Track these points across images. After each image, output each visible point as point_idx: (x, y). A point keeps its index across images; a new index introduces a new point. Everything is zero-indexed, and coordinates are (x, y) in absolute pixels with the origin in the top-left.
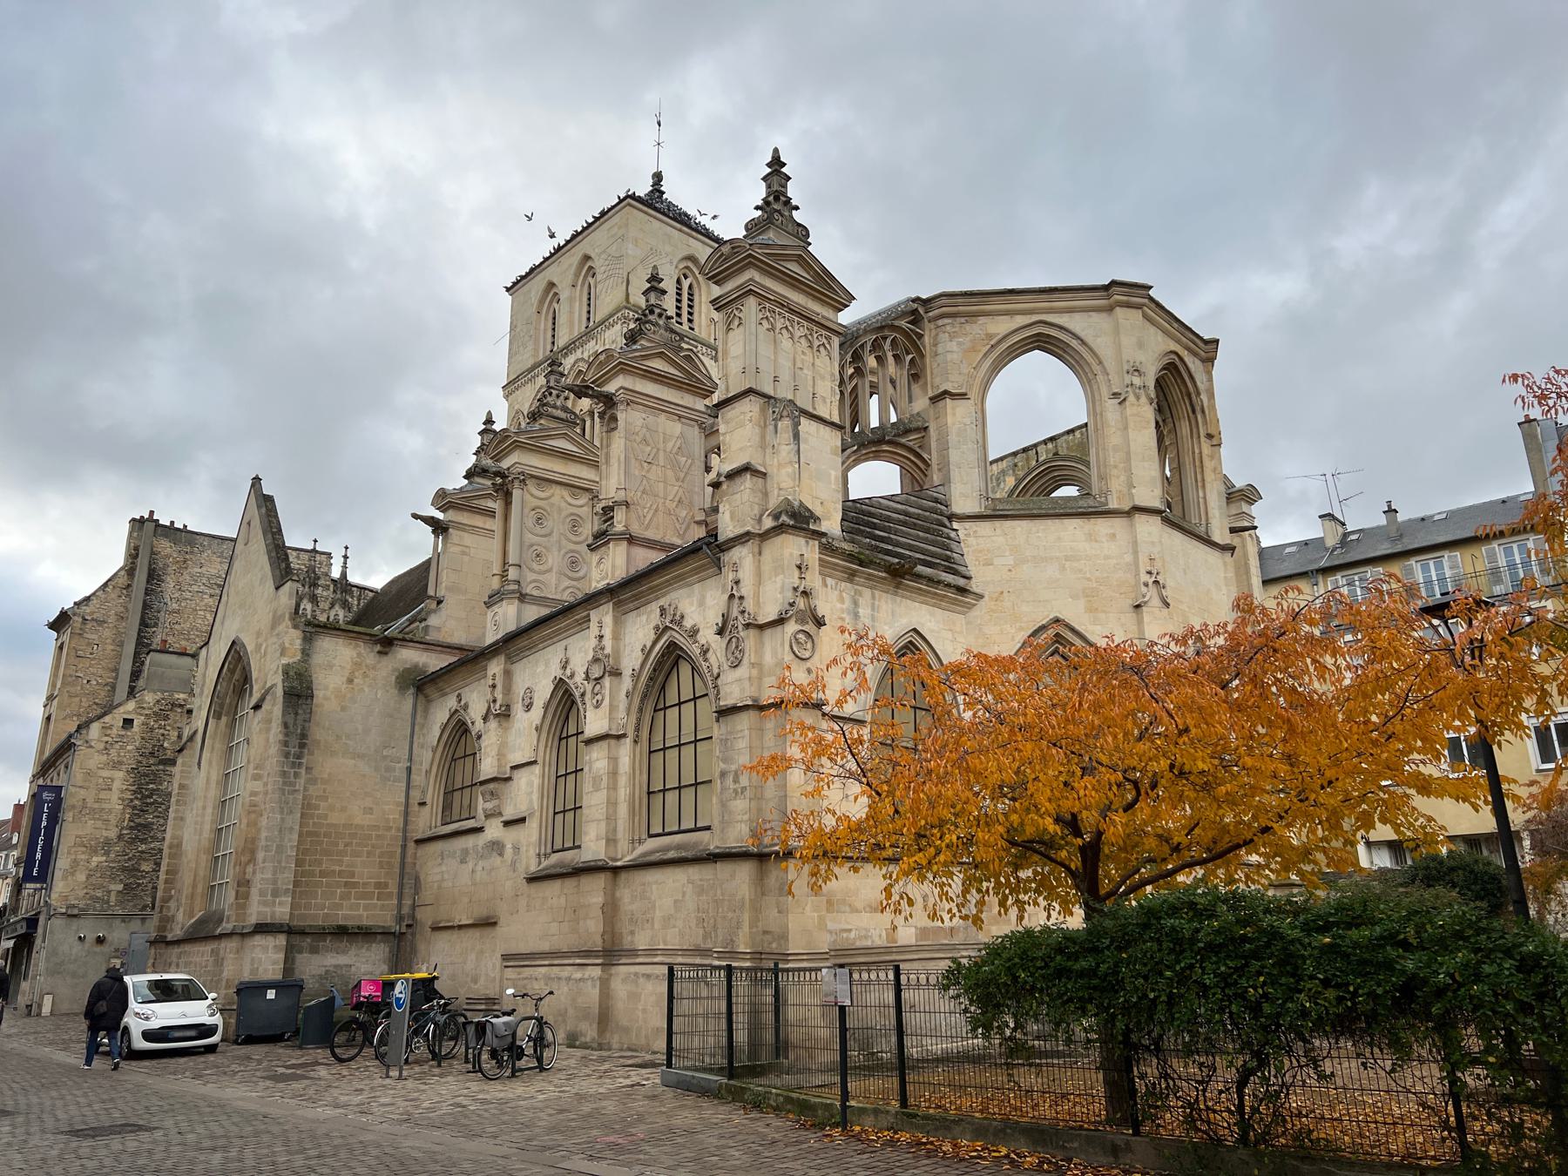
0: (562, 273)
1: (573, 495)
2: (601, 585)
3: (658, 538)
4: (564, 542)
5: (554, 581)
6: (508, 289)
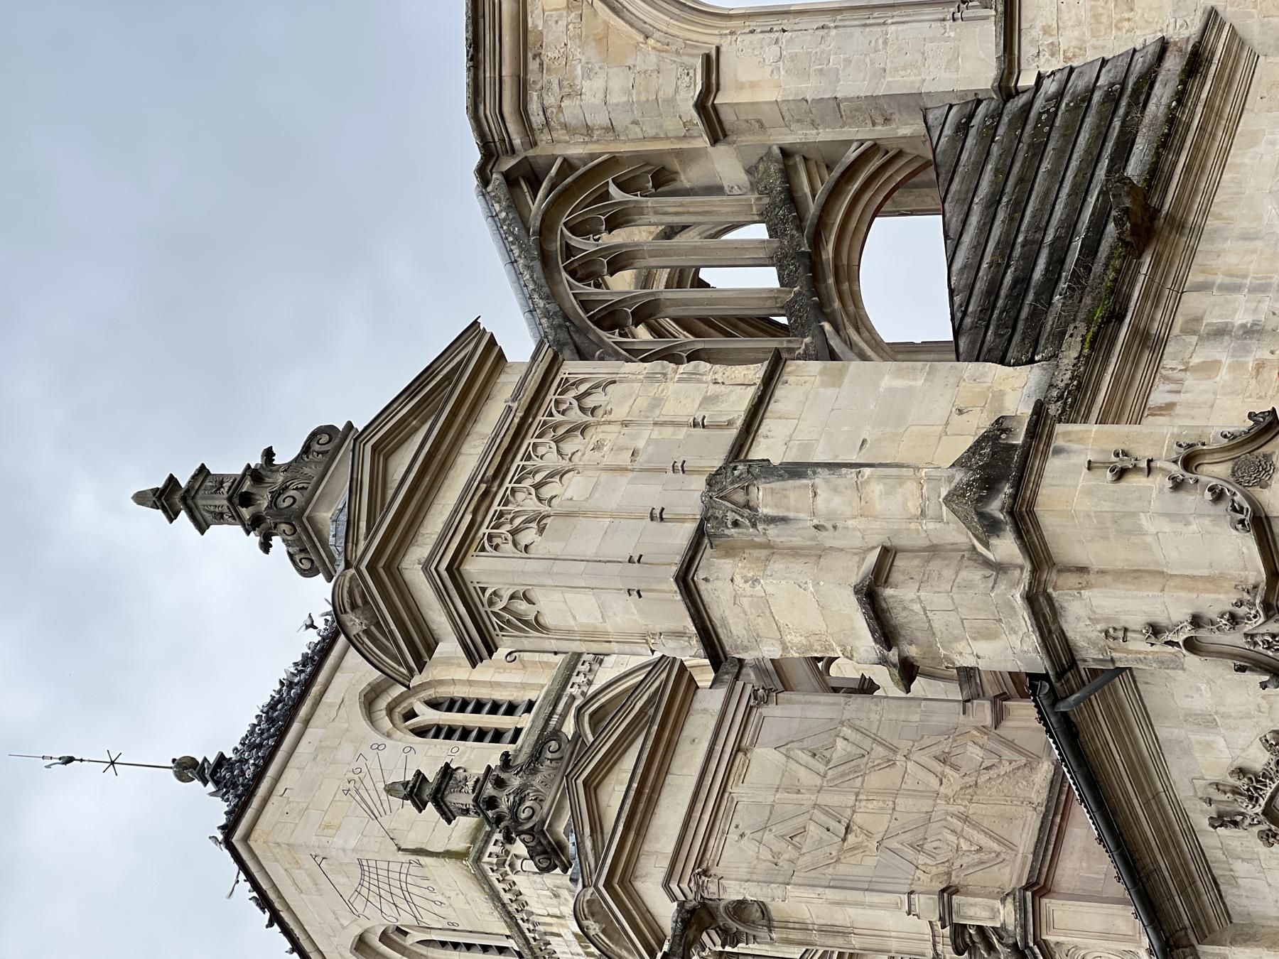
3: (1034, 820)
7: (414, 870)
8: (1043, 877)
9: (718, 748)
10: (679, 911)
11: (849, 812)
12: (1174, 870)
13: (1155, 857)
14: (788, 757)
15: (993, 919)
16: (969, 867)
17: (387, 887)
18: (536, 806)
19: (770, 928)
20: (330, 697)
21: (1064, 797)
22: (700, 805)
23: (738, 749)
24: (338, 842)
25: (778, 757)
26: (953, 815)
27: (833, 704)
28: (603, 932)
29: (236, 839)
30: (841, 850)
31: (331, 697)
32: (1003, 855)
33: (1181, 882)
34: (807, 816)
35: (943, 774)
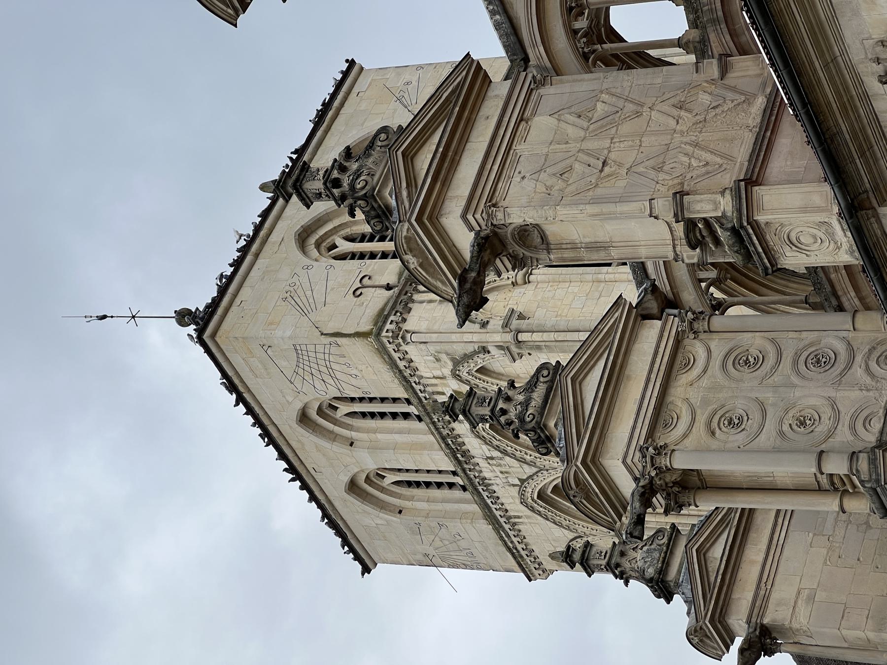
0: (334, 466)
1: (688, 365)
2: (844, 238)
3: (749, 139)
4: (776, 378)
5: (856, 394)
6: (366, 570)
7: (334, 350)
8: (756, 175)
9: (506, 119)
10: (475, 238)
11: (606, 152)
12: (854, 135)
13: (836, 120)
14: (559, 120)
15: (716, 210)
16: (698, 176)
17: (316, 366)
18: (369, 179)
19: (548, 250)
20: (274, 237)
21: (773, 118)
22: (491, 160)
23: (521, 119)
24: (279, 333)
25: (552, 121)
26: (686, 143)
27: (595, 79)
28: (421, 265)
29: (206, 336)
30: (599, 178)
31: (275, 237)
32: (725, 166)
33: (860, 146)
34: (573, 158)
35: (680, 117)
